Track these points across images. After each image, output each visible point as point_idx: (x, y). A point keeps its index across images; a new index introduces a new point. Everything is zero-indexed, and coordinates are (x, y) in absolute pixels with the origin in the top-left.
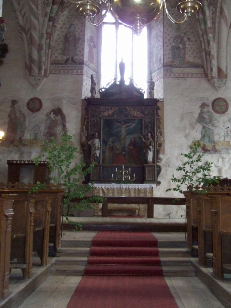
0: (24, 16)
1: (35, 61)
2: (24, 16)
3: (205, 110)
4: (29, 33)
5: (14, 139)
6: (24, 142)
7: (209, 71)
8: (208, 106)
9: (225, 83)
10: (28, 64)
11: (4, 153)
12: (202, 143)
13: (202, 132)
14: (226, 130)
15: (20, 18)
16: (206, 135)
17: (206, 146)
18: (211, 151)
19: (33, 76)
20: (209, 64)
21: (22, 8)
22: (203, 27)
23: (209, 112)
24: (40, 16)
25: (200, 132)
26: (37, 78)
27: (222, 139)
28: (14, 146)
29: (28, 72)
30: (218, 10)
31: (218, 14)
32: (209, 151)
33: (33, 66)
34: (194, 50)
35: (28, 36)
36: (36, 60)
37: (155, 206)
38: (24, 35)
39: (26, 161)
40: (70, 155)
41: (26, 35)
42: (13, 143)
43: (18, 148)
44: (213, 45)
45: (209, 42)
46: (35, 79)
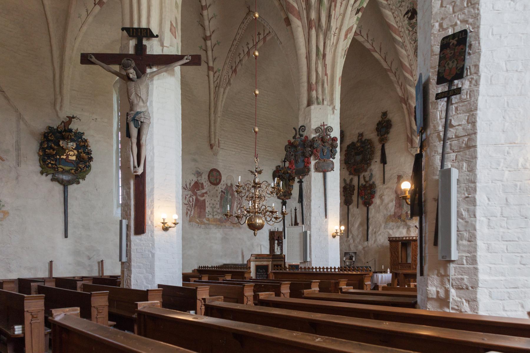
2: (401, 86)
4: (408, 102)
10: (410, 136)
15: (398, 89)
19: (414, 147)
21: (399, 79)
29: (409, 145)
37: (268, 253)
39: (414, 237)
40: (136, 86)
42: (401, 219)
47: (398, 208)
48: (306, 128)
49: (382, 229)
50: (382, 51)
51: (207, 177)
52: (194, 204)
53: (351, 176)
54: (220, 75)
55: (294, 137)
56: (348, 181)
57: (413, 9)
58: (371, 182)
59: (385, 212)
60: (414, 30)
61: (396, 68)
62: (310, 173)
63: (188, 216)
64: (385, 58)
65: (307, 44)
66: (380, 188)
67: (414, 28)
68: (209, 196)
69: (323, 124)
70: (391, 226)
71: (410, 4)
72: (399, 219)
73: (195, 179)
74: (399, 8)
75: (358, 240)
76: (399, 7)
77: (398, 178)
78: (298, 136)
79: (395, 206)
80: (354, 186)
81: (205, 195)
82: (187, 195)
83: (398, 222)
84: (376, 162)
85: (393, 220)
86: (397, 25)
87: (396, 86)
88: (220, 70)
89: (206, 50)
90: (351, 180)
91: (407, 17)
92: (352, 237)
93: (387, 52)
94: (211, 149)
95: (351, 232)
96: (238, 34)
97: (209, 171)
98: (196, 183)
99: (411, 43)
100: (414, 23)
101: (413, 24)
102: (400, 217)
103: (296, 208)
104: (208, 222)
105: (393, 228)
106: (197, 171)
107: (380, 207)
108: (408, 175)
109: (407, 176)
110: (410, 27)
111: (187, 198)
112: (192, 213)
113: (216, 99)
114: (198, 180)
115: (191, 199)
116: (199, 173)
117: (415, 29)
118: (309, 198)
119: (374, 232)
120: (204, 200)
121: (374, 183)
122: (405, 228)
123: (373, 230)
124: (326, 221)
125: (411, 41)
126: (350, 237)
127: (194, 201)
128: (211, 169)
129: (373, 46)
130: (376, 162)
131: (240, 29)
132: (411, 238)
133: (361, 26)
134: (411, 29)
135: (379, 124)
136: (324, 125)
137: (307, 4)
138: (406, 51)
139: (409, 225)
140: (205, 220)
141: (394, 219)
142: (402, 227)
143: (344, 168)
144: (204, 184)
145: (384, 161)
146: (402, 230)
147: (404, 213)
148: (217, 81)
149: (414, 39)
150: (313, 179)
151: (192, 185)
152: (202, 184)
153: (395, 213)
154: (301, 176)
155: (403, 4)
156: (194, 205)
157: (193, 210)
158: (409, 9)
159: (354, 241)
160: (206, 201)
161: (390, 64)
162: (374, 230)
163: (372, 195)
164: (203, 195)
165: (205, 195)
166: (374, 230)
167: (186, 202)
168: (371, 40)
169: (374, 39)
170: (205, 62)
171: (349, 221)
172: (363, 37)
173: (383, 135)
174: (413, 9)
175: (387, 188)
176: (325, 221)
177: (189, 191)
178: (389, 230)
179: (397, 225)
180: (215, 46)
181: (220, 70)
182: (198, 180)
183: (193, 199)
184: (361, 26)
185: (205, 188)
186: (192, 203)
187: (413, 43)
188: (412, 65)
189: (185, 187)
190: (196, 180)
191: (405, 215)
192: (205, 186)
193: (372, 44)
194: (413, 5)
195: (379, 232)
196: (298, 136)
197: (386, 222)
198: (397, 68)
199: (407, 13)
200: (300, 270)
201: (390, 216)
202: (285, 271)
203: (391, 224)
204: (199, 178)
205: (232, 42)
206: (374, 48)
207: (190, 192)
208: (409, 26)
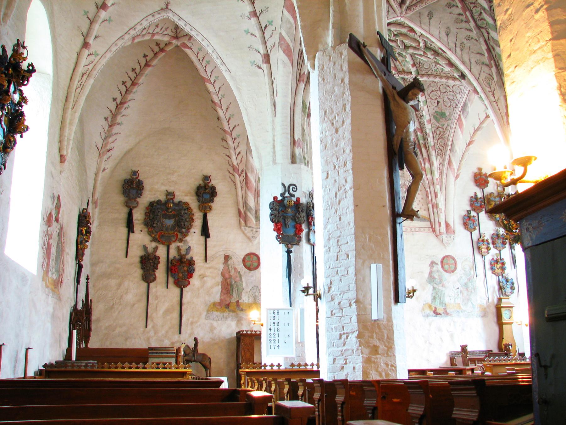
0: (238, 155)
1: (251, 208)
2: (238, 155)
3: (435, 269)
5: (230, 303)
6: (241, 307)
7: (437, 226)
8: (437, 264)
9: (453, 239)
10: (242, 210)
11: (219, 320)
12: (433, 306)
13: (432, 294)
14: (456, 291)
15: (234, 158)
16: (437, 296)
17: (437, 309)
18: (443, 315)
19: (250, 227)
20: (436, 218)
21: (238, 146)
22: (429, 176)
23: (438, 271)
25: (431, 293)
26: (254, 230)
27: (453, 301)
28: (229, 311)
30: (447, 161)
31: (446, 166)
32: (441, 314)
33: (249, 214)
34: (420, 201)
35: (242, 178)
36: (253, 208)
38: (237, 176)
41: (240, 177)
43: (235, 313)
44: (441, 197)
45: (436, 194)
46: (252, 231)
47: (224, 294)
49: (202, 321)
50: (228, 111)
53: (154, 244)
54: (96, 61)
55: (282, 195)
56: (150, 250)
58: (188, 257)
59: (207, 298)
61: (238, 135)
62: (301, 243)
64: (229, 120)
66: (199, 266)
70: (215, 316)
72: (226, 308)
75: (163, 332)
77: (225, 258)
79: (221, 291)
83: (224, 312)
84: (195, 232)
85: (218, 309)
87: (232, 152)
88: (98, 55)
92: (153, 327)
93: (233, 115)
94: (61, 163)
95: (152, 320)
96: (141, 24)
102: (228, 306)
103: (88, 276)
105: (217, 318)
107: (200, 291)
108: (238, 257)
109: (237, 258)
113: (79, 90)
119: (190, 322)
121: (192, 258)
122: (235, 321)
123: (188, 320)
126: (150, 326)
129: (220, 102)
130: (195, 232)
131: (145, 19)
132: (253, 333)
133: (218, 77)
135: (199, 188)
137: (301, 56)
139: (241, 317)
141: (219, 307)
142: (230, 318)
143: (141, 231)
145: (205, 232)
146: (230, 322)
147: (234, 302)
148: (87, 67)
153: (221, 300)
154: (291, 244)
159: (156, 333)
161: (231, 128)
162: (191, 320)
163: (190, 274)
166: (191, 320)
168: (221, 95)
169: (224, 95)
170: (82, 33)
172: (215, 88)
173: (206, 203)
175: (210, 268)
178: (211, 321)
179: (223, 316)
180: (105, 21)
181: (98, 55)
184: (218, 77)
191: (236, 304)
193: (221, 100)
195: (199, 323)
197: (208, 311)
198: (239, 135)
200: (263, 368)
201: (215, 304)
202: (260, 370)
203: (216, 313)
205: (128, 29)
206: (221, 105)
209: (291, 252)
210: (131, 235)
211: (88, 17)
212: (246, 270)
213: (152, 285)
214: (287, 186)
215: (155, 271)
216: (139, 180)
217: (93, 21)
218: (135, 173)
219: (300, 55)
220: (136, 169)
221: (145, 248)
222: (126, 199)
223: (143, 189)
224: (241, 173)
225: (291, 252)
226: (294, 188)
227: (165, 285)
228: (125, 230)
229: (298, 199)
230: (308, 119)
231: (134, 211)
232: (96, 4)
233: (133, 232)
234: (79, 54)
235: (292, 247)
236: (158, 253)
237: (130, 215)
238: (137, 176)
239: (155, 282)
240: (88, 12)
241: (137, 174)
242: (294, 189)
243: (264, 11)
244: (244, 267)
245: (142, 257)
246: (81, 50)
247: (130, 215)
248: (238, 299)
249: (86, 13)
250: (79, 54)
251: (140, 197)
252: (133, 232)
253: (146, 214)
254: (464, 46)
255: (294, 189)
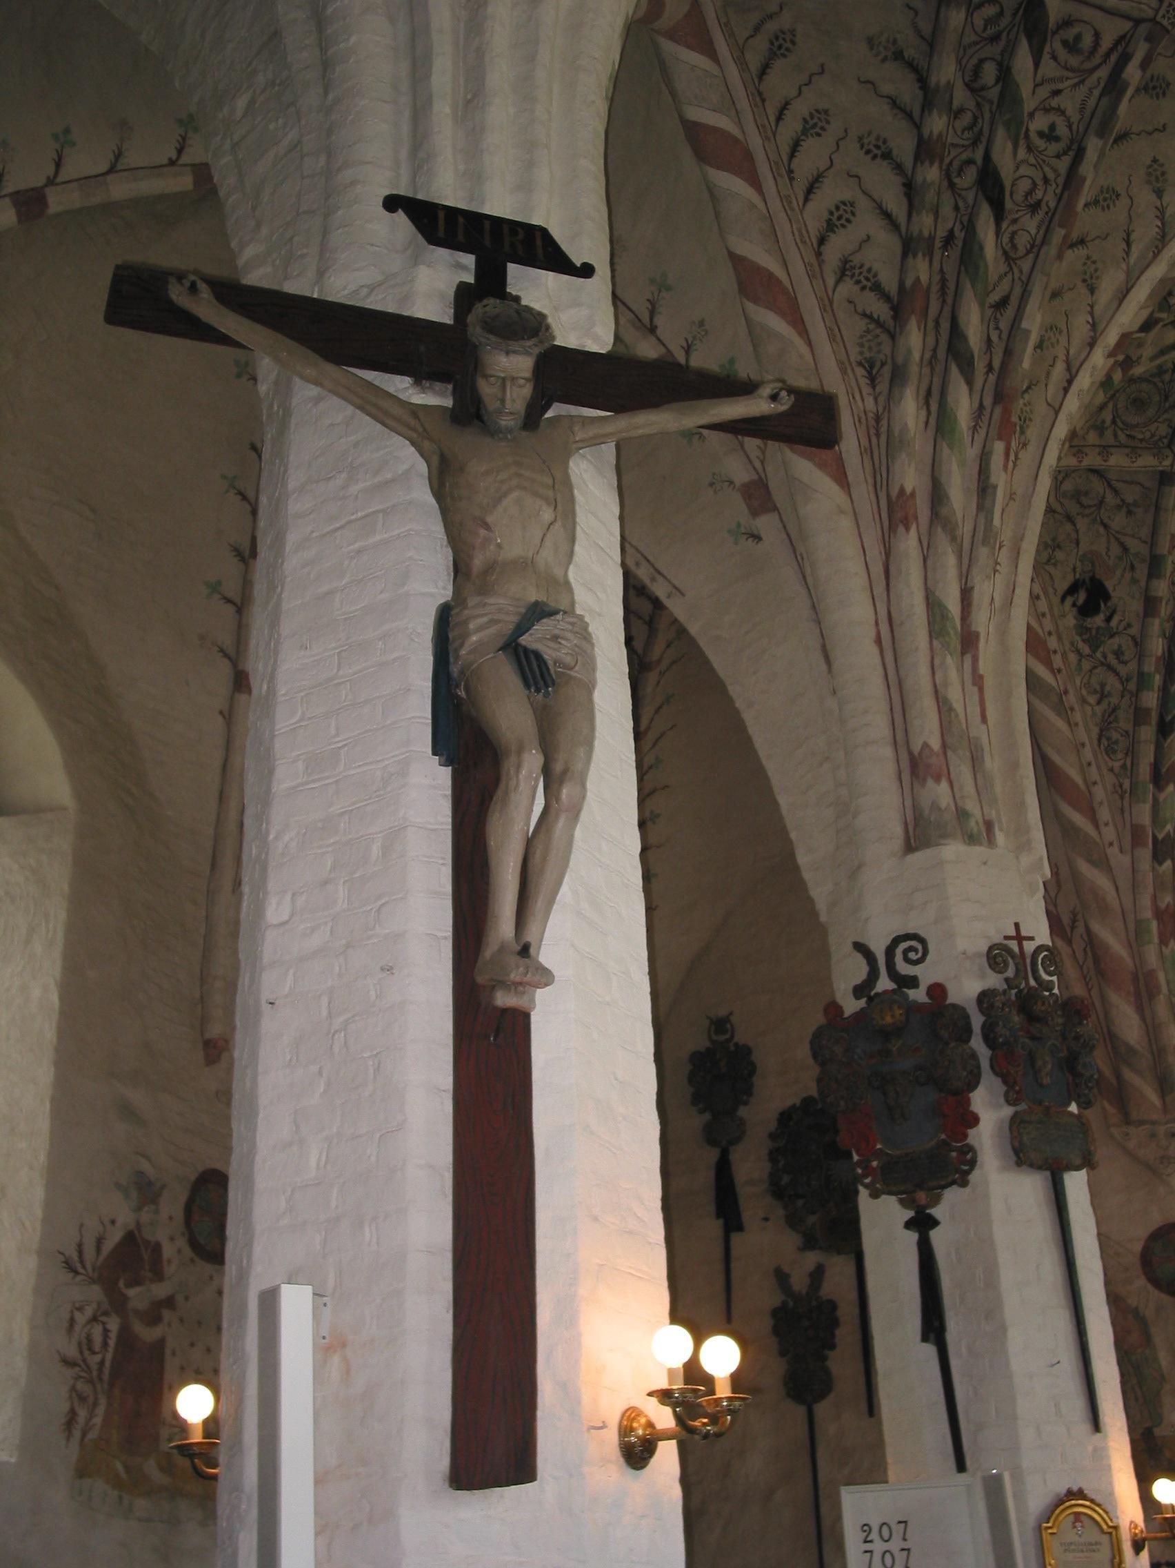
19: (1141, 1123)
24: (1113, 852)
33: (1128, 1075)
35: (1079, 945)
46: (1153, 1135)
48: (931, 947)
51: (179, 1215)
52: (108, 1364)
53: (812, 1259)
56: (799, 1282)
57: (1093, 579)
60: (1099, 655)
62: (974, 1177)
63: (77, 1434)
65: (880, 589)
67: (1098, 647)
68: (181, 1320)
69: (1012, 933)
71: (1080, 561)
73: (125, 1217)
74: (1047, 567)
76: (1046, 563)
78: (884, 984)
80: (833, 1306)
81: (167, 1314)
82: (80, 1309)
86: (1041, 625)
89: (238, 601)
90: (817, 1275)
91: (1074, 605)
97: (193, 1178)
98: (131, 1239)
99: (1084, 701)
100: (1098, 628)
101: (1094, 632)
104: (164, 1480)
106: (141, 1174)
110: (1083, 641)
111: (77, 1328)
112: (98, 1420)
114: (138, 1225)
115: (97, 1331)
116: (150, 1184)
117: (1101, 649)
118: (992, 1311)
120: (161, 1343)
124: (1095, 1450)
125: (1084, 692)
127: (112, 1343)
128: (201, 1169)
134: (1086, 650)
136: (1019, 938)
138: (1070, 725)
140: (151, 1467)
143: (766, 1219)
144: (168, 1251)
149: (1098, 688)
150: (997, 1207)
151: (108, 1247)
152: (157, 1248)
155: (1060, 555)
156: (107, 1371)
157: (103, 1402)
158: (1078, 576)
160: (168, 1352)
164: (153, 1316)
165: (167, 1314)
167: (72, 1352)
170: (222, 650)
171: (821, 1486)
174: (1093, 579)
176: (1090, 1449)
177: (93, 1281)
182: (138, 1225)
183: (106, 1332)
185: (169, 1270)
186: (98, 1358)
187: (1092, 699)
188: (1095, 783)
189: (75, 1256)
190: (132, 1226)
192: (169, 1262)
194: (1093, 565)
196: (884, 984)
199: (1073, 589)
204: (145, 1216)
207: (96, 1293)
208: (1078, 638)
209: (934, 1223)
210: (736, 1238)
211: (225, 598)
212: (1163, 1296)
213: (823, 1409)
214: (878, 947)
215: (825, 1359)
216: (736, 1045)
217: (242, 604)
218: (721, 1025)
219: (873, 431)
220: (722, 1012)
221: (781, 1277)
222: (707, 1116)
223: (752, 1072)
224: (1073, 928)
225: (934, 1223)
226: (911, 949)
227: (864, 1406)
228: (714, 1227)
229: (937, 991)
230: (968, 659)
231: (736, 1155)
232: (236, 550)
233: (740, 1228)
234: (230, 715)
235: (936, 1200)
236: (828, 1289)
237: (723, 1171)
238: (729, 1034)
239: (831, 1398)
240: (219, 583)
241: (728, 1026)
242: (912, 955)
243: (694, 338)
244: (1150, 1287)
245: (775, 1313)
246: (232, 698)
247: (723, 1171)
248: (1147, 1425)
249: (214, 587)
250: (230, 715)
251: (746, 1103)
252: (740, 1228)
253: (773, 1156)
254: (788, 50)
255: (912, 955)
